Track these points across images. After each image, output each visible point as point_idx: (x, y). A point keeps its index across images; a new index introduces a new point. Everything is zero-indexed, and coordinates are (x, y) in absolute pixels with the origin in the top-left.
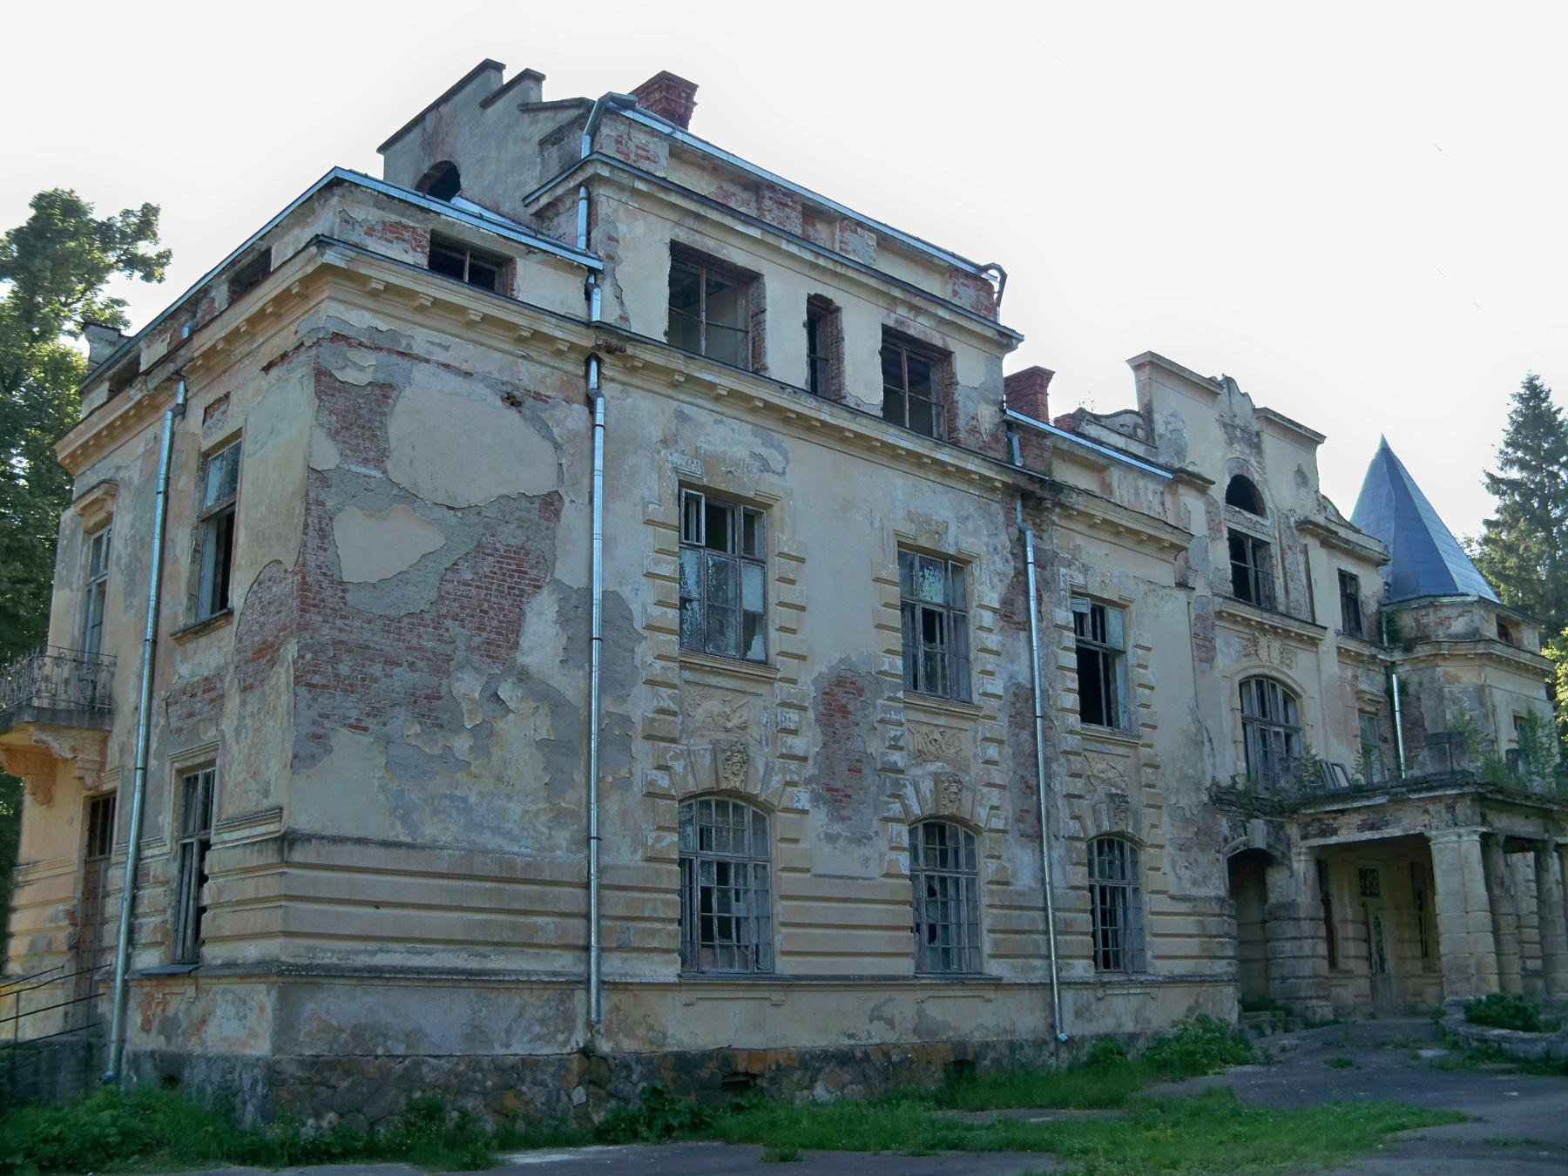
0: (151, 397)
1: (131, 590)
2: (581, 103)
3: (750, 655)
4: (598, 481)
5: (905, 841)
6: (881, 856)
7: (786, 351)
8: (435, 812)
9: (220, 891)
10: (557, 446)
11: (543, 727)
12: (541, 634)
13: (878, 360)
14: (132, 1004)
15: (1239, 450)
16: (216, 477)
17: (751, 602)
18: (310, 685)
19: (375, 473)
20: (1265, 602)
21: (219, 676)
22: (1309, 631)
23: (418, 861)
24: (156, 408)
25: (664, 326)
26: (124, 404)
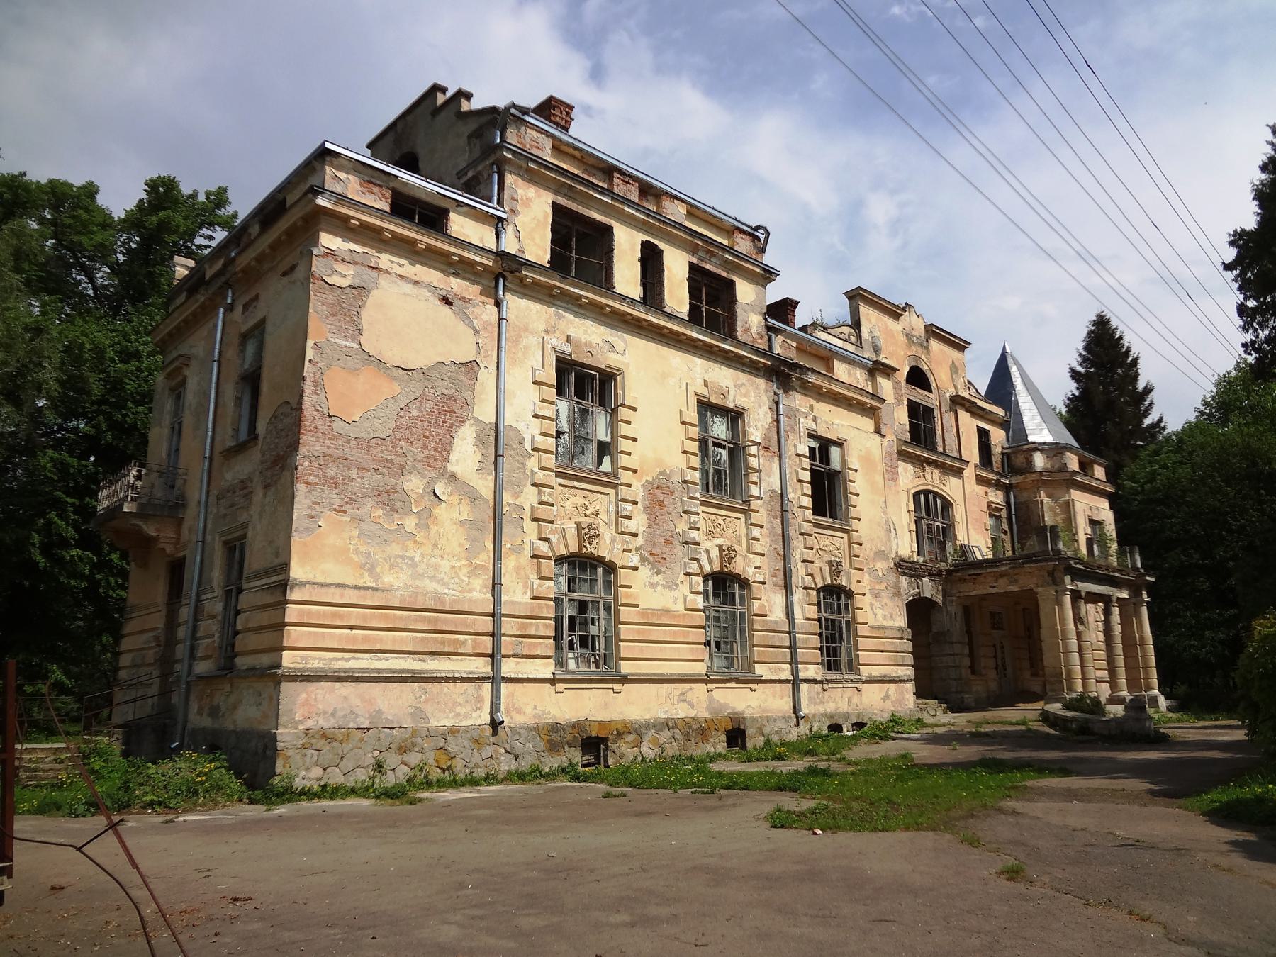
2: (493, 110)
3: (602, 468)
5: (701, 589)
6: (685, 597)
8: (391, 567)
10: (476, 331)
11: (465, 511)
12: (466, 454)
13: (686, 284)
14: (192, 697)
15: (915, 350)
16: (251, 349)
17: (603, 435)
19: (352, 345)
20: (931, 446)
24: (216, 309)
25: (548, 257)
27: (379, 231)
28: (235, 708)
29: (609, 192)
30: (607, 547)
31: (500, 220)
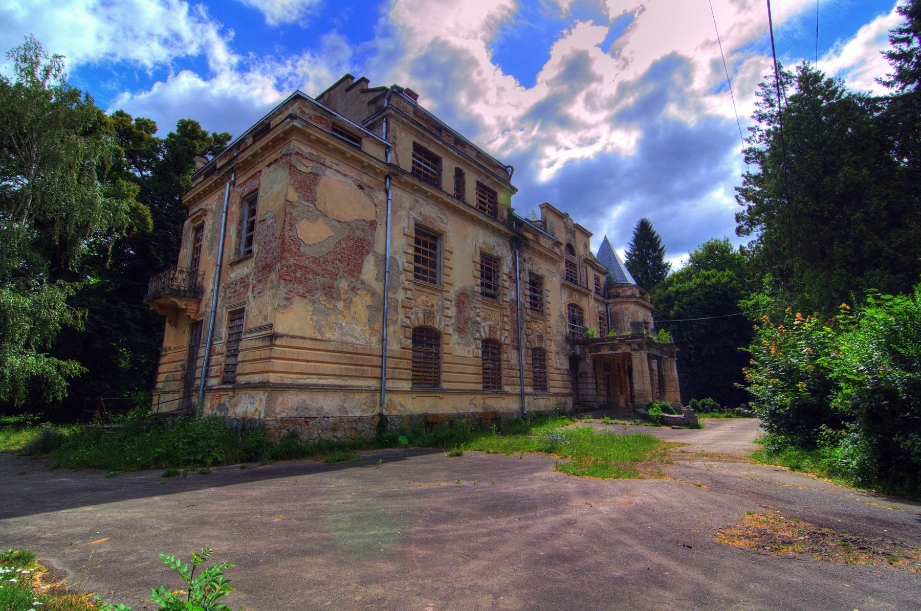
0: (221, 179)
1: (211, 248)
4: (389, 218)
7: (448, 182)
8: (330, 328)
9: (245, 356)
12: (369, 270)
18: (285, 280)
21: (247, 277)
22: (587, 292)
23: (322, 346)
24: (223, 183)
26: (210, 182)
27: (326, 144)
28: (236, 405)
29: (439, 139)
30: (439, 323)
31: (388, 147)
